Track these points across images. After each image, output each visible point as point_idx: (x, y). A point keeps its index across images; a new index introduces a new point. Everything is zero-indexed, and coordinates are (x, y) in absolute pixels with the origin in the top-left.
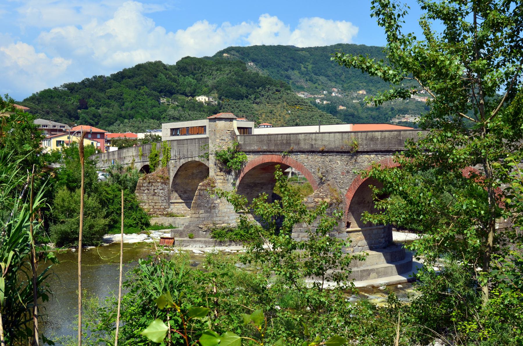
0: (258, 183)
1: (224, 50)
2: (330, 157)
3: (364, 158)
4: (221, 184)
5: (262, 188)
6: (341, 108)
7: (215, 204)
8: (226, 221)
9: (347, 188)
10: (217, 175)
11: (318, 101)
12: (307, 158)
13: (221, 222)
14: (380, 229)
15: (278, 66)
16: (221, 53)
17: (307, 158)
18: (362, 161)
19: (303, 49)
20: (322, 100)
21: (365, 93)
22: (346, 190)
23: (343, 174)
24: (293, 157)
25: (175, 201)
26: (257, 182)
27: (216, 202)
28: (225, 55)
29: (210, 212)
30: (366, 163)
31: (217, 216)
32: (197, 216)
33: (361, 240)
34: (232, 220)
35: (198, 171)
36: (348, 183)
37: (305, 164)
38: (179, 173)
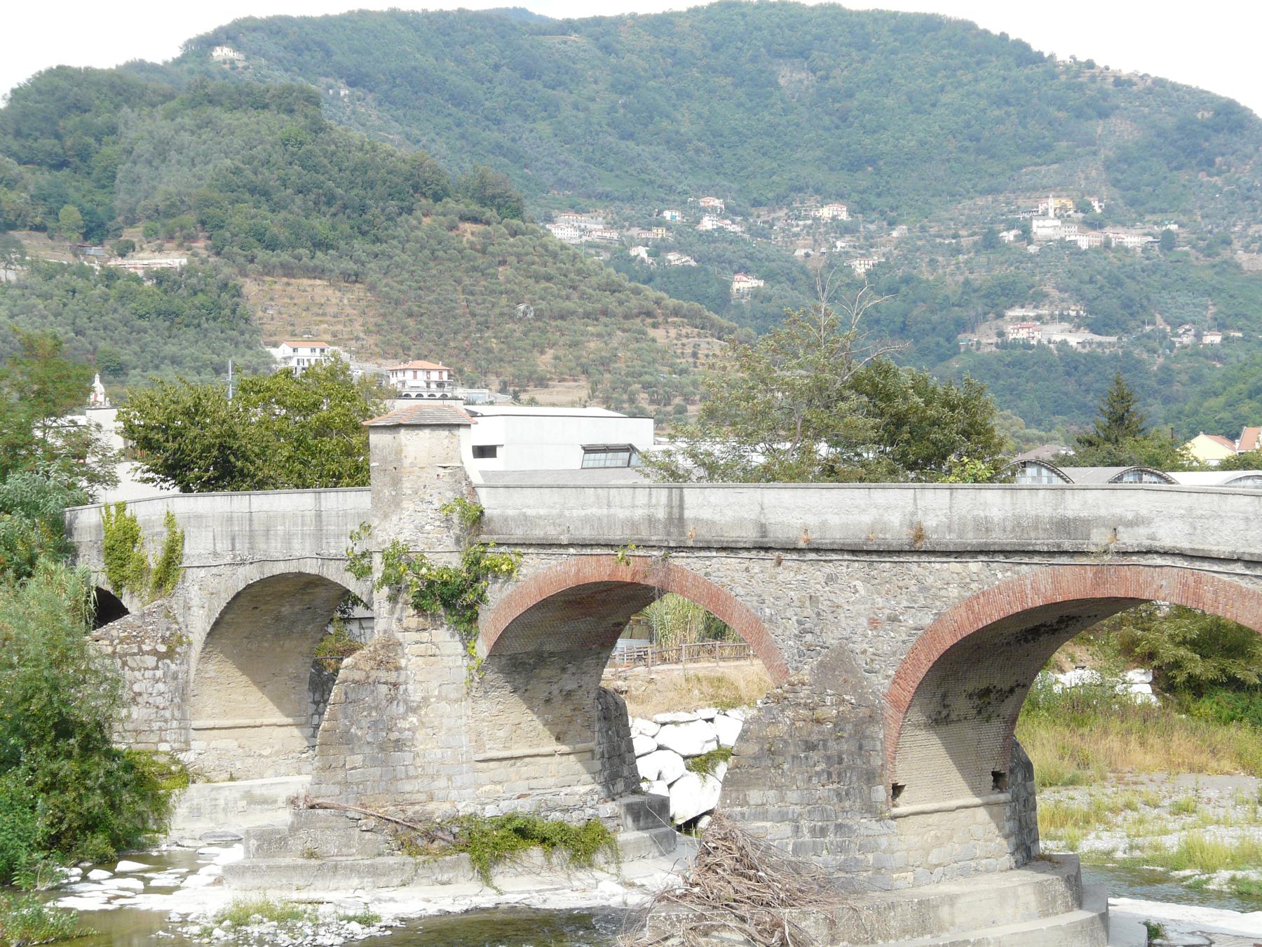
0: (552, 654)
1: (221, 30)
2: (828, 569)
3: (946, 575)
4: (420, 661)
5: (564, 670)
6: (743, 284)
7: (401, 731)
8: (441, 794)
9: (891, 672)
10: (406, 630)
11: (641, 252)
12: (747, 570)
13: (422, 797)
14: (997, 804)
15: (459, 100)
16: (206, 43)
17: (747, 570)
18: (939, 584)
19: (568, 27)
20: (657, 250)
21: (844, 216)
22: (888, 677)
23: (874, 623)
24: (680, 561)
25: (211, 723)
26: (549, 647)
27: (402, 724)
28: (222, 53)
29: (384, 763)
30: (954, 591)
31: (408, 777)
32: (340, 776)
33: (1063, 817)
34: (461, 788)
35: (297, 609)
36: (894, 654)
37: (740, 590)
38: (227, 617)
